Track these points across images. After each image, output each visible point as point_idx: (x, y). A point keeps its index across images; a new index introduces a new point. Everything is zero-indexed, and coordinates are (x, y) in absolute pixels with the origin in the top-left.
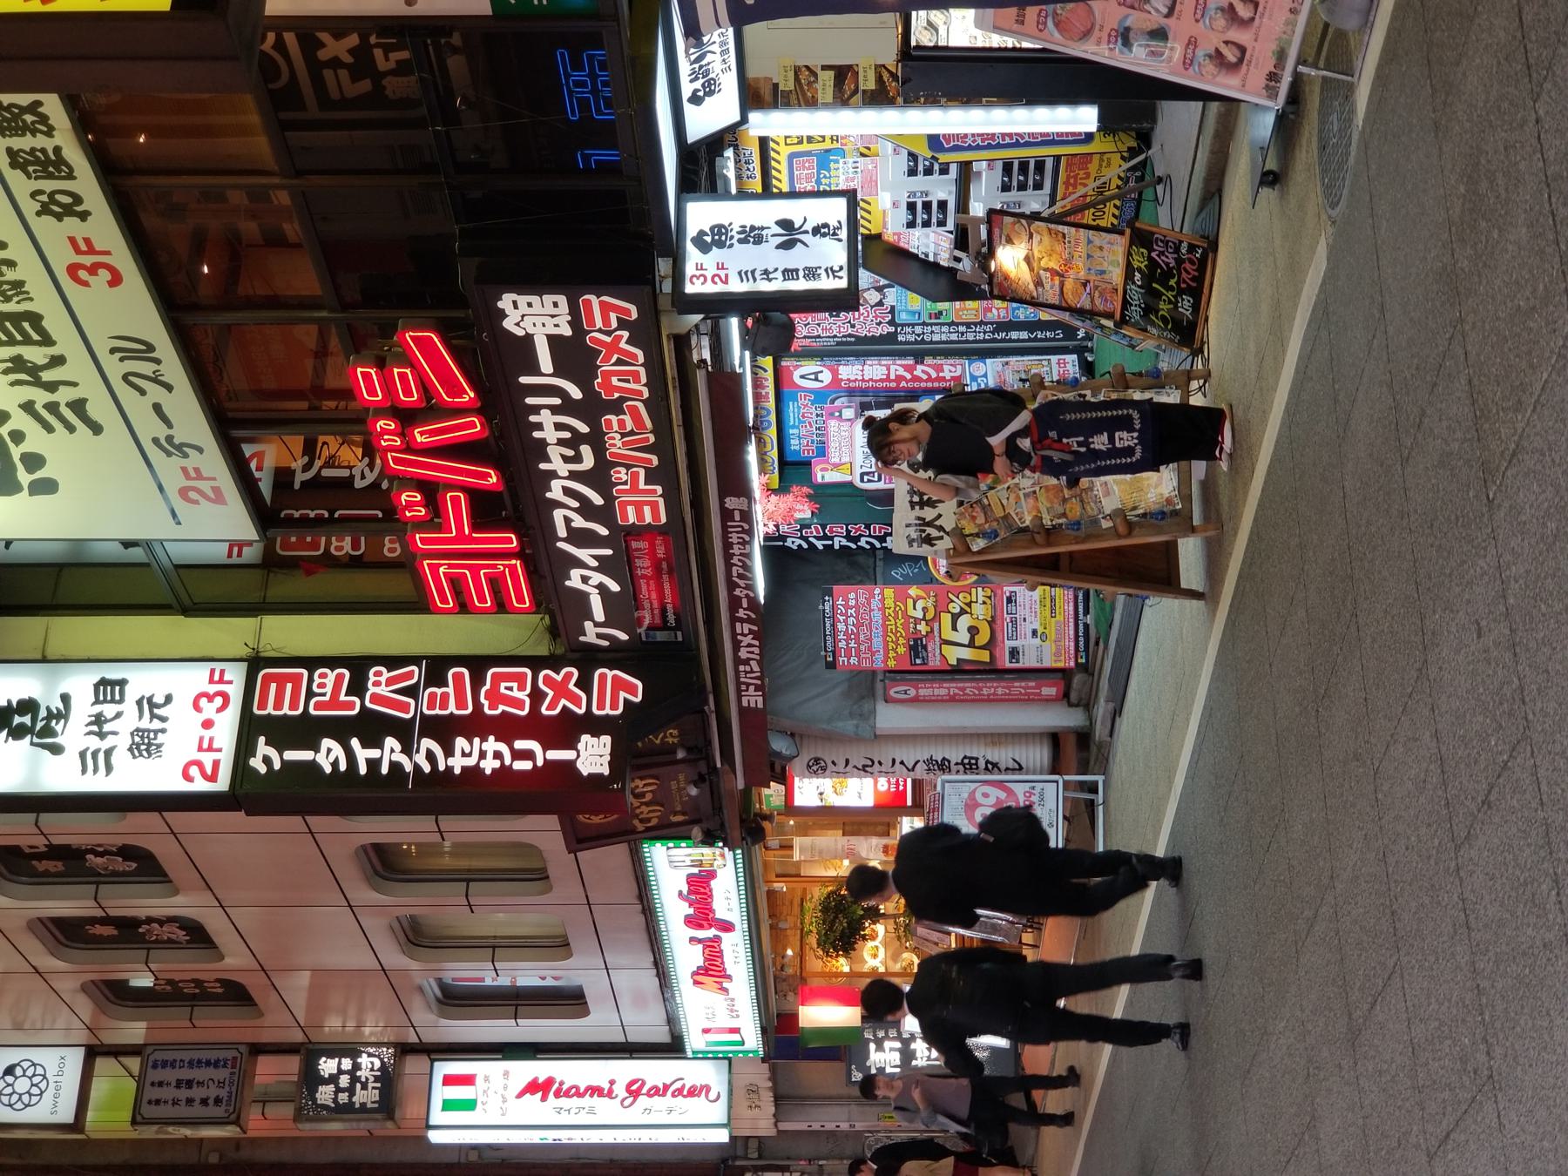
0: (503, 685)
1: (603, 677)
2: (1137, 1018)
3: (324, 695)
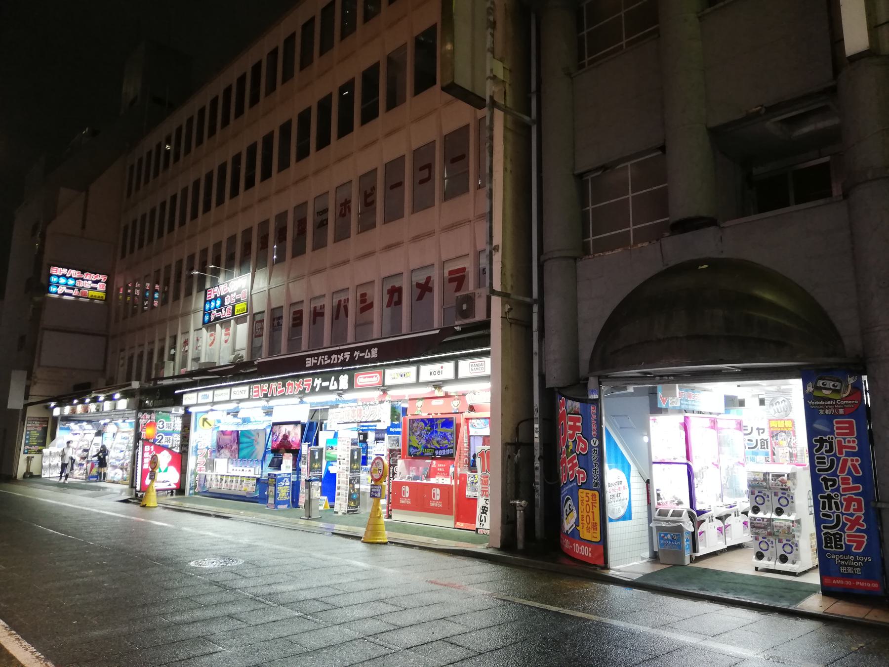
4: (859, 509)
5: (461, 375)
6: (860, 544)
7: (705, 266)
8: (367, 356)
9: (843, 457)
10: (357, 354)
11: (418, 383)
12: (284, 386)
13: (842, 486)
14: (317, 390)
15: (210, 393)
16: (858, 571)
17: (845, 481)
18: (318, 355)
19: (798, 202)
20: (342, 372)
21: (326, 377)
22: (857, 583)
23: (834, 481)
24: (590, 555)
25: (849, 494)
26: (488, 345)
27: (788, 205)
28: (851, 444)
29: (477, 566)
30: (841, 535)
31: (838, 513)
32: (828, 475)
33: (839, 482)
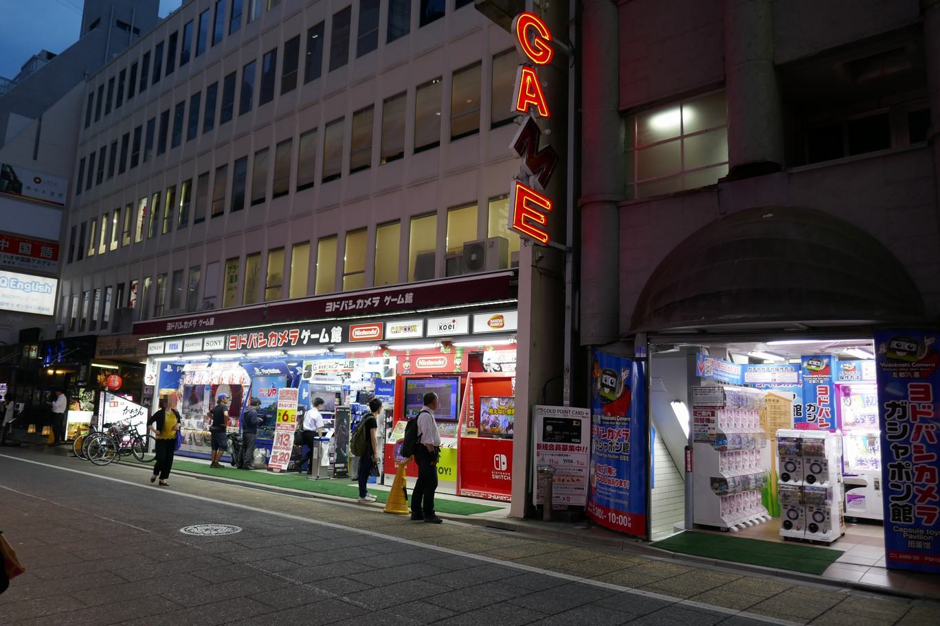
0: (929, 473)
2: (435, 502)
4: (932, 480)
5: (477, 330)
7: (770, 215)
8: (400, 301)
9: (917, 423)
10: (387, 299)
11: (425, 338)
12: (266, 337)
13: (915, 455)
14: (305, 342)
15: (180, 343)
16: (928, 546)
17: (918, 449)
18: (341, 299)
19: (853, 153)
20: (336, 324)
21: (316, 329)
22: (926, 558)
23: (906, 449)
24: (630, 525)
25: (922, 463)
26: (515, 296)
27: (842, 156)
30: (911, 507)
31: (909, 483)
32: (900, 442)
33: (911, 450)
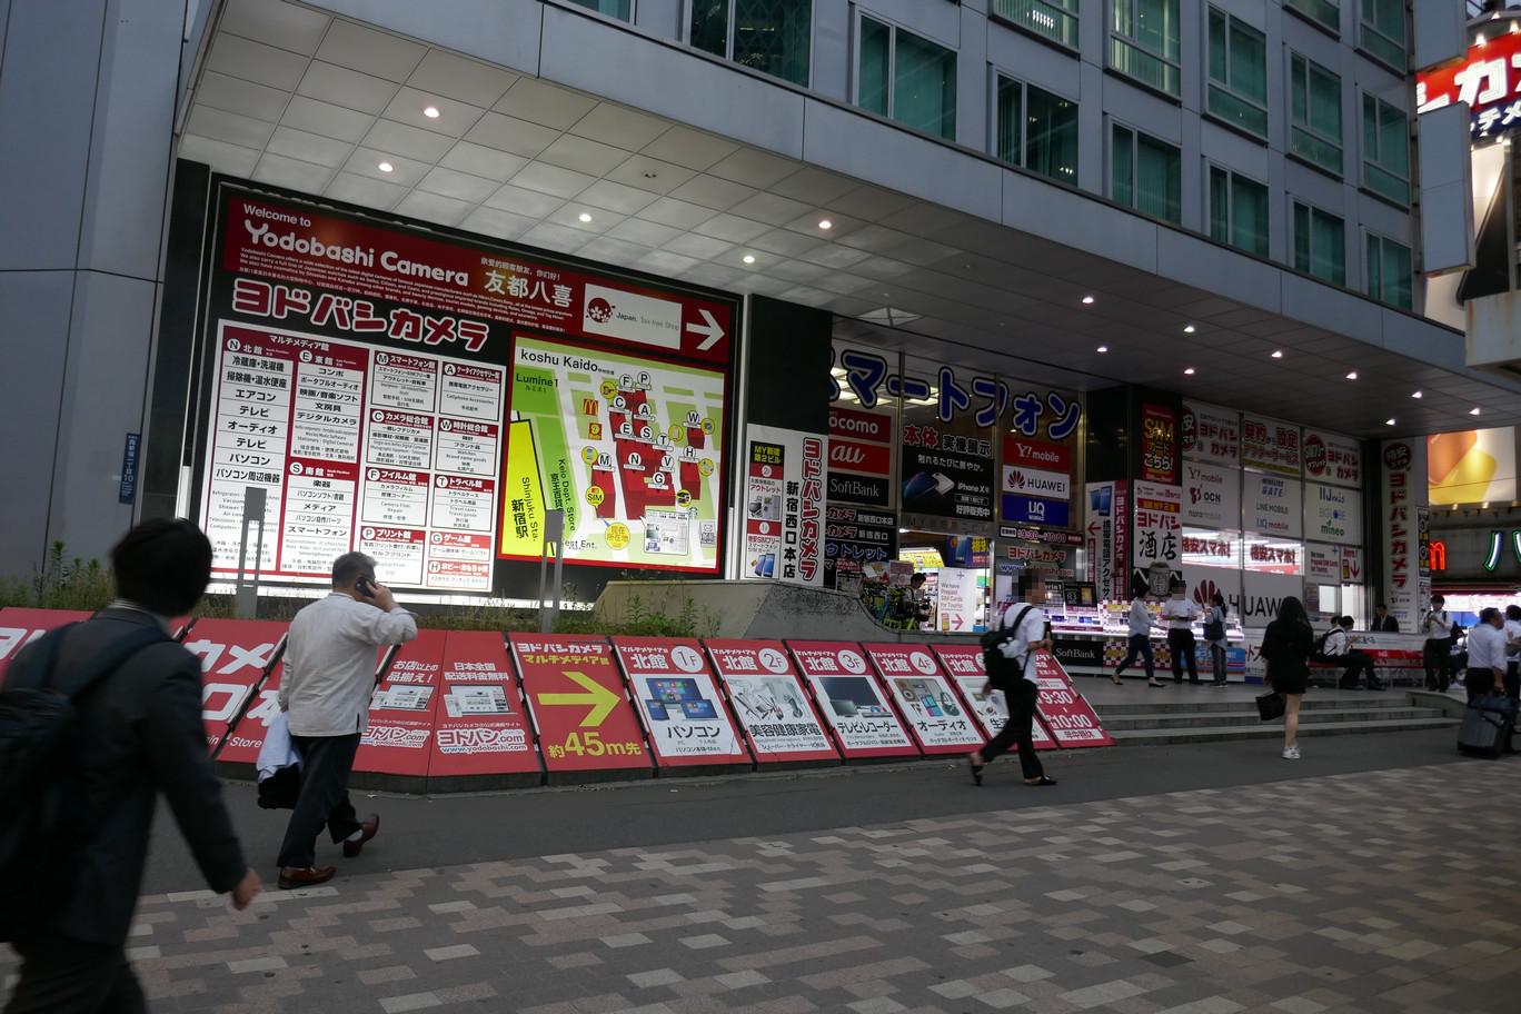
0: (411, 324)
1: (484, 329)
3: (290, 295)
6: (478, 338)
28: (300, 300)
29: (1352, 492)
